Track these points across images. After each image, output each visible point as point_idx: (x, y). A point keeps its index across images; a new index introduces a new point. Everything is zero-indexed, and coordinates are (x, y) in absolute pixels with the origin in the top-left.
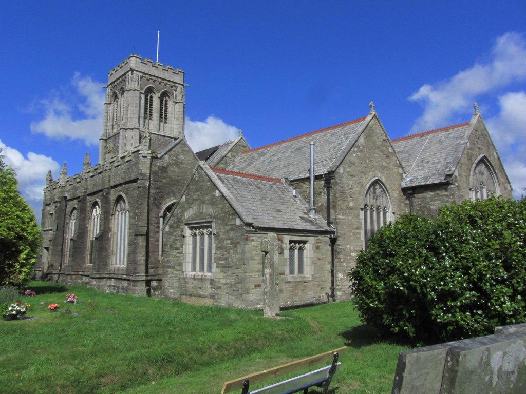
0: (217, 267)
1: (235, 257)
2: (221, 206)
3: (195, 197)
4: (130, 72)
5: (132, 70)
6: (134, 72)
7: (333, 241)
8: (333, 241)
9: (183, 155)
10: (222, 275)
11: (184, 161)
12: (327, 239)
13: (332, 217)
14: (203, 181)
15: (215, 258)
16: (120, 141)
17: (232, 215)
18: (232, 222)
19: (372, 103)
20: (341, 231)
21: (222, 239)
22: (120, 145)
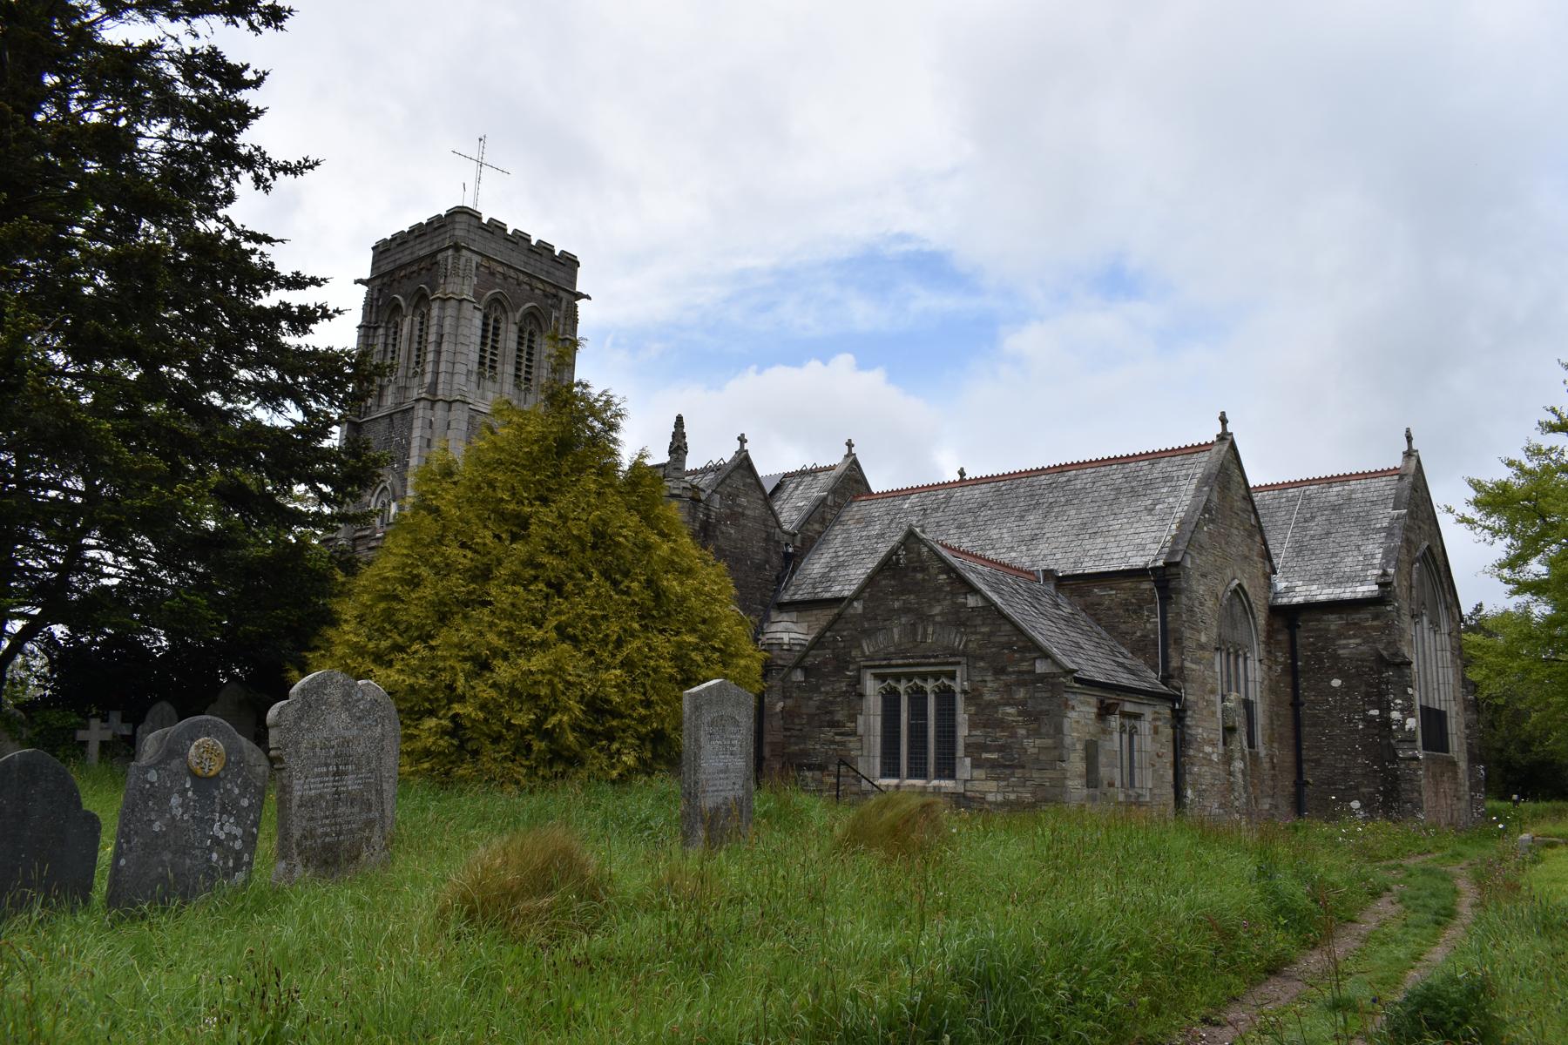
0: (975, 766)
1: (1032, 745)
2: (985, 629)
3: (897, 605)
4: (450, 252)
5: (457, 248)
6: (464, 252)
7: (1178, 718)
8: (1178, 718)
9: (746, 494)
10: (992, 785)
11: (748, 512)
12: (1166, 711)
13: (1174, 663)
14: (924, 570)
15: (967, 746)
16: (416, 433)
17: (1022, 650)
18: (1025, 666)
19: (164, 369)
20: (1191, 694)
21: (989, 703)
22: (415, 443)
